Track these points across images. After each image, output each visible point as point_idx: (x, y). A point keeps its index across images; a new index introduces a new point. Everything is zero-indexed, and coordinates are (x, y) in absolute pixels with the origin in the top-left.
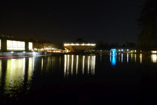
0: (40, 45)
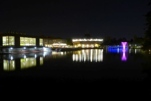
0: (50, 41)
